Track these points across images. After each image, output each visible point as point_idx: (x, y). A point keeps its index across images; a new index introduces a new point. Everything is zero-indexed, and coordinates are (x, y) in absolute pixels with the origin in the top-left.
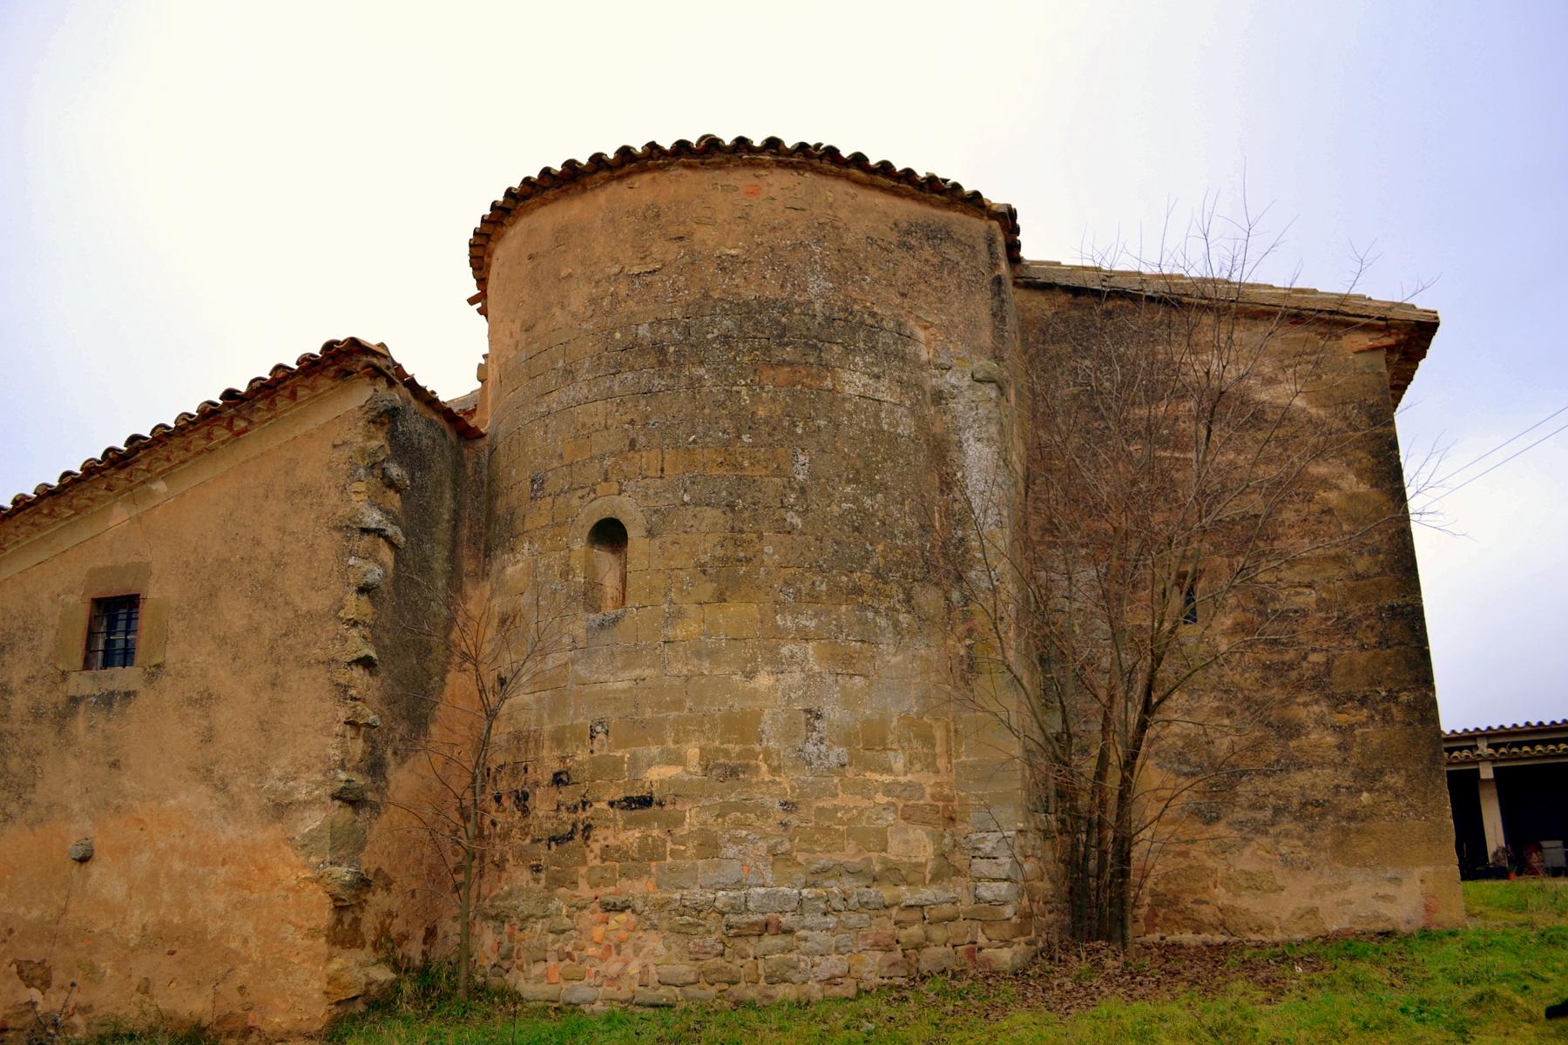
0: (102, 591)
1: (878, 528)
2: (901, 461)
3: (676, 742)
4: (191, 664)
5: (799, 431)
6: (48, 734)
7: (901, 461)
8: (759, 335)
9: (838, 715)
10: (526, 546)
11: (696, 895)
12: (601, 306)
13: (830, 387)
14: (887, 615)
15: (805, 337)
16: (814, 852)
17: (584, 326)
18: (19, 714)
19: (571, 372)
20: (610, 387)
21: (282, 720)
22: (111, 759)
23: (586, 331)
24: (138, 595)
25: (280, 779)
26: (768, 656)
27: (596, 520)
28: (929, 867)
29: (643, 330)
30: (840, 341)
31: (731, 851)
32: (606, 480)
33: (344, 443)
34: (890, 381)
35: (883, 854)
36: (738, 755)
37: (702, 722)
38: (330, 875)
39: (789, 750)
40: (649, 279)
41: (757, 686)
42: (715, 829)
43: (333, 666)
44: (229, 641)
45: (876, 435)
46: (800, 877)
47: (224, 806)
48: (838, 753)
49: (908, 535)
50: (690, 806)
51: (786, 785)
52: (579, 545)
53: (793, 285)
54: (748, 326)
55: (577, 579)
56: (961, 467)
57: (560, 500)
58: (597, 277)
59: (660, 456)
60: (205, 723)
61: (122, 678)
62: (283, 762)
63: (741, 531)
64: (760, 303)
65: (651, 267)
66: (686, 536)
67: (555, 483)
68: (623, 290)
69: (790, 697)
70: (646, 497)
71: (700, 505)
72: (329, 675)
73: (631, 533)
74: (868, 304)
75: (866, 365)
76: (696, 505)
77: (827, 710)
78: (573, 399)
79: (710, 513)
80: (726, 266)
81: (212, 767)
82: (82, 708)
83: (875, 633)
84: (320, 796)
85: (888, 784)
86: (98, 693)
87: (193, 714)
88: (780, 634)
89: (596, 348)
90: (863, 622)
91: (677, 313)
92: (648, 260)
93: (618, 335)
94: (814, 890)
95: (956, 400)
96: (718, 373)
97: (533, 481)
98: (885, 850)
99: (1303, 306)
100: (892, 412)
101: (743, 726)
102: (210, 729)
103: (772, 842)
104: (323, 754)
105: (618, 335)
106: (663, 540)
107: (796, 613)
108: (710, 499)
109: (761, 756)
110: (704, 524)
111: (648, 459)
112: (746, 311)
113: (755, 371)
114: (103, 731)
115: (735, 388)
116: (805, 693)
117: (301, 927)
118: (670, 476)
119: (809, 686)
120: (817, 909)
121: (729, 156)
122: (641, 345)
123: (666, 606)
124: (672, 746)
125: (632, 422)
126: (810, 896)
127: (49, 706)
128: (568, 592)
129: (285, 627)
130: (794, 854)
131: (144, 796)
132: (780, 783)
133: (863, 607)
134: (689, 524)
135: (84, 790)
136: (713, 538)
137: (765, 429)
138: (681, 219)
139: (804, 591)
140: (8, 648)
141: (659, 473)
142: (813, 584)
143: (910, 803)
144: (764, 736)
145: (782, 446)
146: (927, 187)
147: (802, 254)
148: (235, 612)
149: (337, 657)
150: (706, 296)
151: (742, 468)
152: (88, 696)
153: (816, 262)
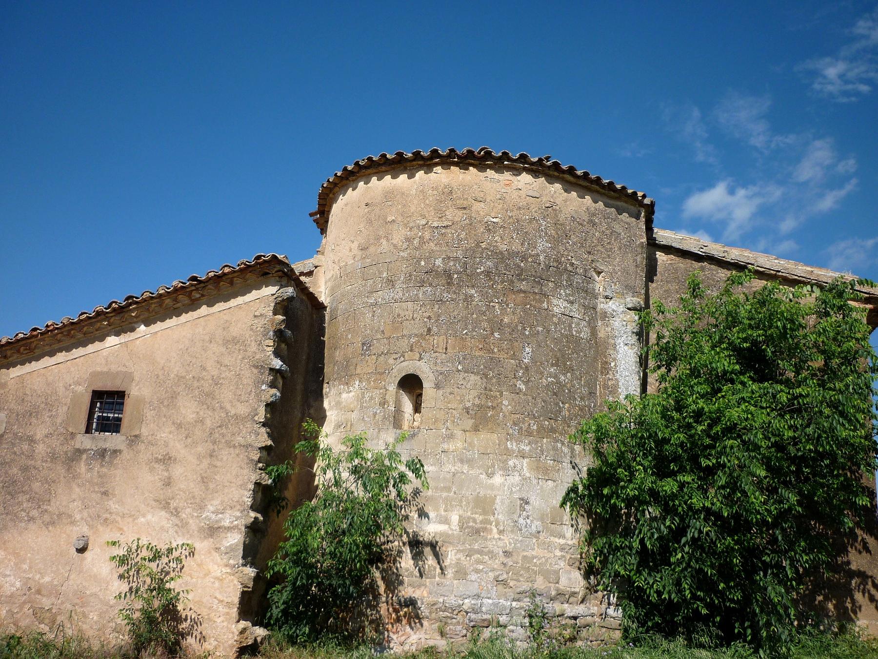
0: (100, 386)
1: (567, 394)
2: (581, 354)
3: (445, 511)
4: (158, 437)
5: (527, 333)
6: (61, 470)
7: (581, 354)
9: (538, 503)
10: (357, 383)
11: (452, 601)
13: (546, 307)
14: (568, 446)
15: (534, 276)
16: (519, 581)
17: (402, 254)
18: (40, 456)
19: (391, 281)
20: (417, 295)
21: (216, 477)
22: (103, 490)
23: (402, 257)
24: (124, 392)
25: (212, 512)
27: (404, 374)
28: (581, 594)
29: (439, 262)
30: (553, 280)
31: (473, 577)
32: (411, 350)
34: (579, 306)
35: (557, 585)
36: (481, 522)
37: (461, 500)
39: (509, 521)
40: (443, 231)
41: (494, 482)
42: (465, 563)
44: (183, 426)
45: (570, 338)
47: (176, 525)
48: (536, 525)
49: (582, 399)
50: (451, 548)
52: (392, 388)
53: (528, 244)
54: (501, 267)
55: (390, 408)
56: (614, 360)
57: (382, 358)
58: (411, 225)
59: (445, 340)
60: (166, 474)
61: (110, 440)
62: (216, 502)
63: (491, 390)
64: (509, 254)
65: (445, 224)
66: (458, 390)
67: (379, 346)
68: (427, 235)
69: (512, 490)
70: (436, 364)
71: (467, 372)
72: (247, 454)
74: (570, 258)
75: (567, 295)
76: (465, 372)
77: (532, 500)
78: (393, 298)
79: (473, 377)
80: (490, 228)
82: (84, 456)
83: (561, 456)
84: (238, 525)
85: (563, 545)
86: (95, 449)
87: (159, 468)
88: (508, 453)
90: (555, 449)
91: (460, 254)
92: (444, 219)
93: (423, 263)
94: (519, 603)
95: (614, 319)
97: (363, 344)
98: (558, 583)
99: (820, 280)
100: (578, 324)
101: (484, 505)
102: (169, 478)
103: (497, 574)
104: (241, 500)
105: (423, 263)
107: (518, 441)
108: (474, 369)
109: (494, 523)
111: (438, 341)
112: (501, 257)
113: (504, 294)
114: (98, 472)
115: (492, 304)
117: (222, 601)
119: (523, 485)
120: (519, 615)
121: (496, 161)
122: (437, 271)
123: (444, 430)
125: (429, 318)
126: (517, 607)
127: (62, 453)
129: (220, 422)
130: (509, 581)
131: (124, 514)
133: (556, 440)
134: (461, 383)
135: (83, 507)
136: (474, 393)
138: (465, 196)
140: (34, 414)
141: (444, 351)
142: (529, 425)
143: (573, 556)
144: (496, 512)
145: (517, 341)
146: (607, 187)
147: (534, 225)
148: (188, 409)
151: (493, 352)
152: (89, 450)
153: (542, 230)
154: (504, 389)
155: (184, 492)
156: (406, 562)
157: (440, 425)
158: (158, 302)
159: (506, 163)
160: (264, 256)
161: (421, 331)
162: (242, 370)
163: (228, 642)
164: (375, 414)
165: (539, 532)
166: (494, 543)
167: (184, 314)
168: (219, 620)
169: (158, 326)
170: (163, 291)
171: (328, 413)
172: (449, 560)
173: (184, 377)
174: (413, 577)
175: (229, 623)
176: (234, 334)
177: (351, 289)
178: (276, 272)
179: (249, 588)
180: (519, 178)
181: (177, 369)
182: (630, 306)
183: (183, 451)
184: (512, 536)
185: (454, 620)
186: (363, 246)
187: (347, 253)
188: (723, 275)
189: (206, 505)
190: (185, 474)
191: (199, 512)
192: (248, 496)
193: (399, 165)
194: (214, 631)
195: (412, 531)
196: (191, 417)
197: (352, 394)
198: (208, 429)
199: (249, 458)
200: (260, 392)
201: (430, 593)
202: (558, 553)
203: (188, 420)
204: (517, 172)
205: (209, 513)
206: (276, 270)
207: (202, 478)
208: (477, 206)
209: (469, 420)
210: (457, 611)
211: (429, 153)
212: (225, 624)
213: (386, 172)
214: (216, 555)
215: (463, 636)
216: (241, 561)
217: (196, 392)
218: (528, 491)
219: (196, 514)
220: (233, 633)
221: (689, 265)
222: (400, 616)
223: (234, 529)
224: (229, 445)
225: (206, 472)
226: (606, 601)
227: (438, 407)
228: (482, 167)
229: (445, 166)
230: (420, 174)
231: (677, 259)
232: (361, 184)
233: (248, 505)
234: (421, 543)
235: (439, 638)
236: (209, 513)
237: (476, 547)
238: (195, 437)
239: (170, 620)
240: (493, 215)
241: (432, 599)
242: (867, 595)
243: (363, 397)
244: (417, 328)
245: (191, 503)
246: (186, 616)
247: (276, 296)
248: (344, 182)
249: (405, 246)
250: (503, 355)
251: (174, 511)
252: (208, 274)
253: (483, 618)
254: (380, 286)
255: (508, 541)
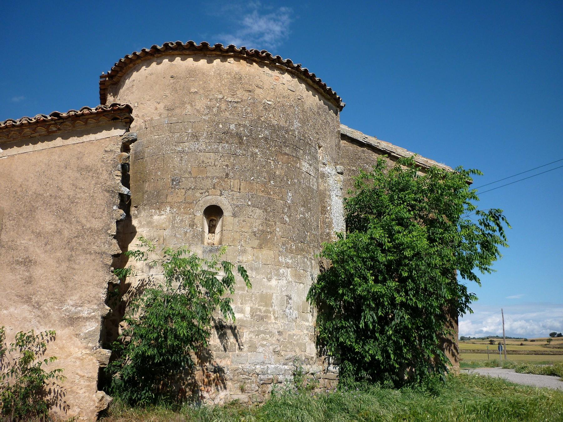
8: (279, 141)
10: (168, 208)
11: (247, 367)
12: (212, 111)
20: (217, 148)
23: (204, 120)
25: (72, 306)
26: (276, 272)
27: (208, 205)
29: (232, 127)
31: (260, 349)
32: (214, 188)
33: (111, 151)
37: (252, 296)
38: (100, 353)
40: (235, 105)
42: (255, 340)
43: (104, 255)
46: (283, 361)
51: (279, 325)
53: (289, 122)
54: (274, 135)
56: (330, 205)
57: (190, 192)
60: (27, 274)
62: (75, 298)
63: (269, 221)
65: (236, 100)
67: (188, 183)
68: (223, 106)
71: (255, 207)
73: (225, 213)
76: (253, 207)
77: (293, 297)
78: (198, 149)
79: (258, 211)
80: (267, 108)
81: (31, 296)
88: (279, 264)
89: (210, 129)
92: (235, 96)
93: (221, 126)
96: (264, 153)
97: (173, 180)
98: (305, 351)
101: (266, 299)
103: (274, 347)
104: (97, 296)
105: (221, 126)
106: (239, 219)
109: (272, 313)
110: (256, 215)
111: (234, 183)
112: (275, 129)
115: (269, 161)
116: (287, 289)
117: (83, 376)
118: (243, 192)
122: (231, 133)
123: (239, 247)
124: (240, 306)
125: (227, 166)
128: (194, 234)
129: (76, 233)
132: (277, 324)
137: (278, 180)
139: (289, 248)
142: (291, 246)
145: (284, 188)
149: (107, 251)
150: (259, 119)
154: (277, 220)
155: (45, 289)
156: (214, 340)
157: (237, 244)
158: (18, 130)
159: (277, 64)
160: (119, 105)
161: (221, 175)
162: (95, 193)
163: (89, 408)
164: (186, 233)
165: (296, 318)
166: (272, 326)
167: (40, 143)
168: (81, 392)
169: (15, 150)
170: (26, 122)
171: (137, 230)
172: (244, 339)
173: (42, 195)
174: (219, 351)
175: (90, 393)
176: (87, 164)
177: (158, 138)
178: (125, 118)
179: (106, 365)
180: (283, 76)
181: (35, 187)
182: (339, 171)
183: (42, 256)
184: (283, 321)
185: (249, 380)
186: (169, 107)
187: (153, 111)
188: (376, 157)
189: (66, 300)
190: (46, 274)
191: (59, 305)
192: (103, 292)
193: (200, 52)
194: (77, 401)
195: (217, 318)
196: (49, 228)
197: (164, 216)
198: (65, 239)
199: (104, 263)
200: (112, 211)
201: (232, 362)
202: (306, 332)
203: (47, 230)
204: (283, 71)
205: (69, 305)
206: (125, 116)
207: (62, 278)
208: (258, 91)
209: (256, 240)
210: (252, 374)
211: (162, 46)
212: (87, 394)
213: (189, 56)
214: (77, 341)
215: (256, 391)
216: (98, 344)
217: (54, 208)
218: (291, 290)
219: (57, 307)
220: (94, 401)
221: (355, 148)
222: (211, 380)
223: (93, 319)
224: (86, 251)
225: (65, 273)
226: (327, 361)
227: (235, 230)
228: (261, 64)
229: (236, 59)
230: (217, 62)
231: (348, 144)
232: (166, 61)
233: (103, 300)
234: (225, 327)
235: (240, 393)
236: (69, 305)
237: (262, 329)
238: (54, 245)
239: (35, 393)
240: (268, 99)
241: (234, 366)
242: (451, 351)
243: (174, 220)
244: (218, 172)
245: (52, 299)
246: (50, 389)
247: (123, 137)
248: (149, 57)
249: (206, 111)
250: (276, 197)
251: (36, 305)
252: (69, 113)
253: (269, 378)
254: (186, 138)
255: (280, 324)
